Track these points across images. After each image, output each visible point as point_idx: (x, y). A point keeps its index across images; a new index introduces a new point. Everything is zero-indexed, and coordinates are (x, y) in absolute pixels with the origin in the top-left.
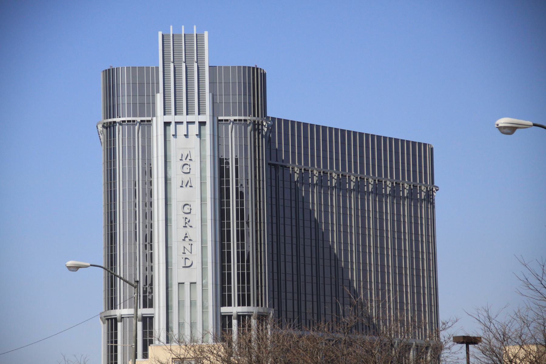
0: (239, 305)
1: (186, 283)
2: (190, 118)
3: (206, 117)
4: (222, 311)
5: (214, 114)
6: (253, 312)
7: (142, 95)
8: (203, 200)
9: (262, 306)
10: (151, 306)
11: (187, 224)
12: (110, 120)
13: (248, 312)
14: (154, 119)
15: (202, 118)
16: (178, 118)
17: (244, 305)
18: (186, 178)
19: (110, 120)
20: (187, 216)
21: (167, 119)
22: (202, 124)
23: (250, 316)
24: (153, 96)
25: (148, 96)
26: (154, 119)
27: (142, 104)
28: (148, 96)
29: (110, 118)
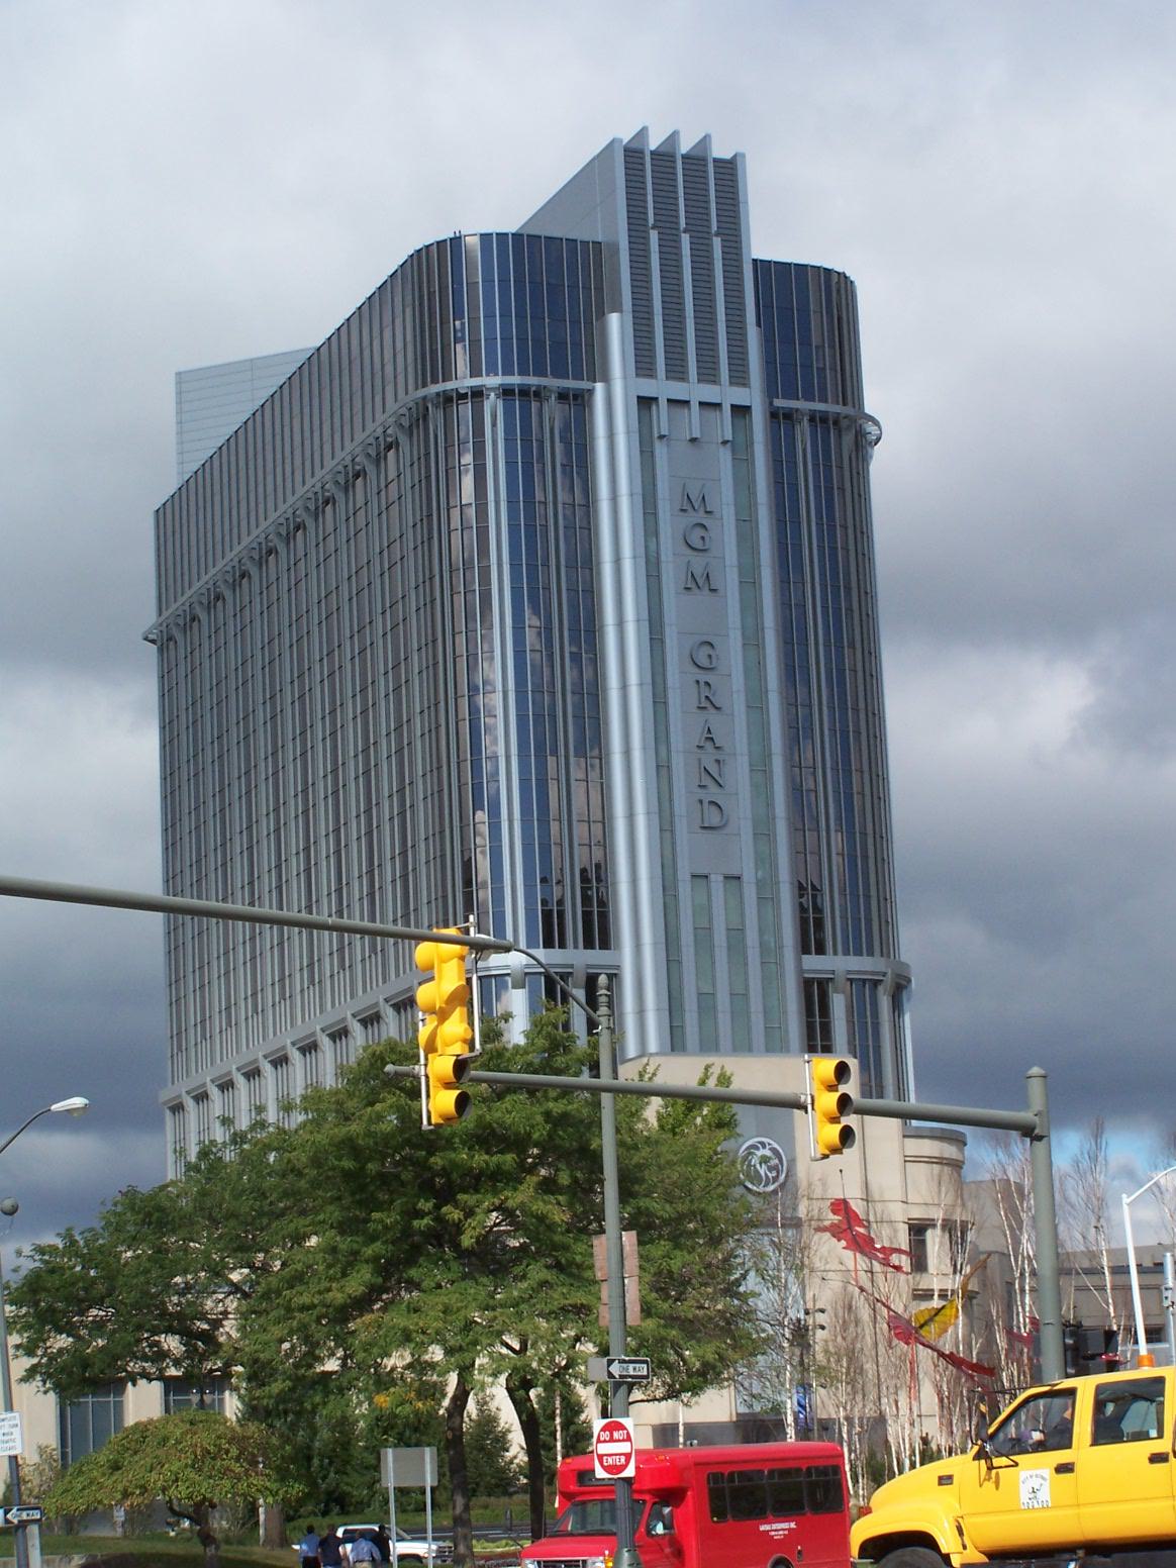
0: (846, 953)
1: (713, 877)
2: (709, 393)
3: (753, 395)
4: (805, 967)
5: (771, 391)
6: (884, 974)
7: (557, 319)
8: (753, 641)
9: (889, 957)
10: (605, 944)
11: (709, 703)
12: (434, 389)
13: (873, 973)
14: (599, 387)
15: (739, 396)
16: (677, 390)
17: (858, 953)
18: (698, 563)
19: (434, 389)
20: (703, 677)
21: (648, 388)
22: (741, 411)
23: (876, 983)
24: (589, 323)
25: (575, 322)
26: (599, 387)
27: (559, 346)
28: (575, 322)
29: (435, 381)
